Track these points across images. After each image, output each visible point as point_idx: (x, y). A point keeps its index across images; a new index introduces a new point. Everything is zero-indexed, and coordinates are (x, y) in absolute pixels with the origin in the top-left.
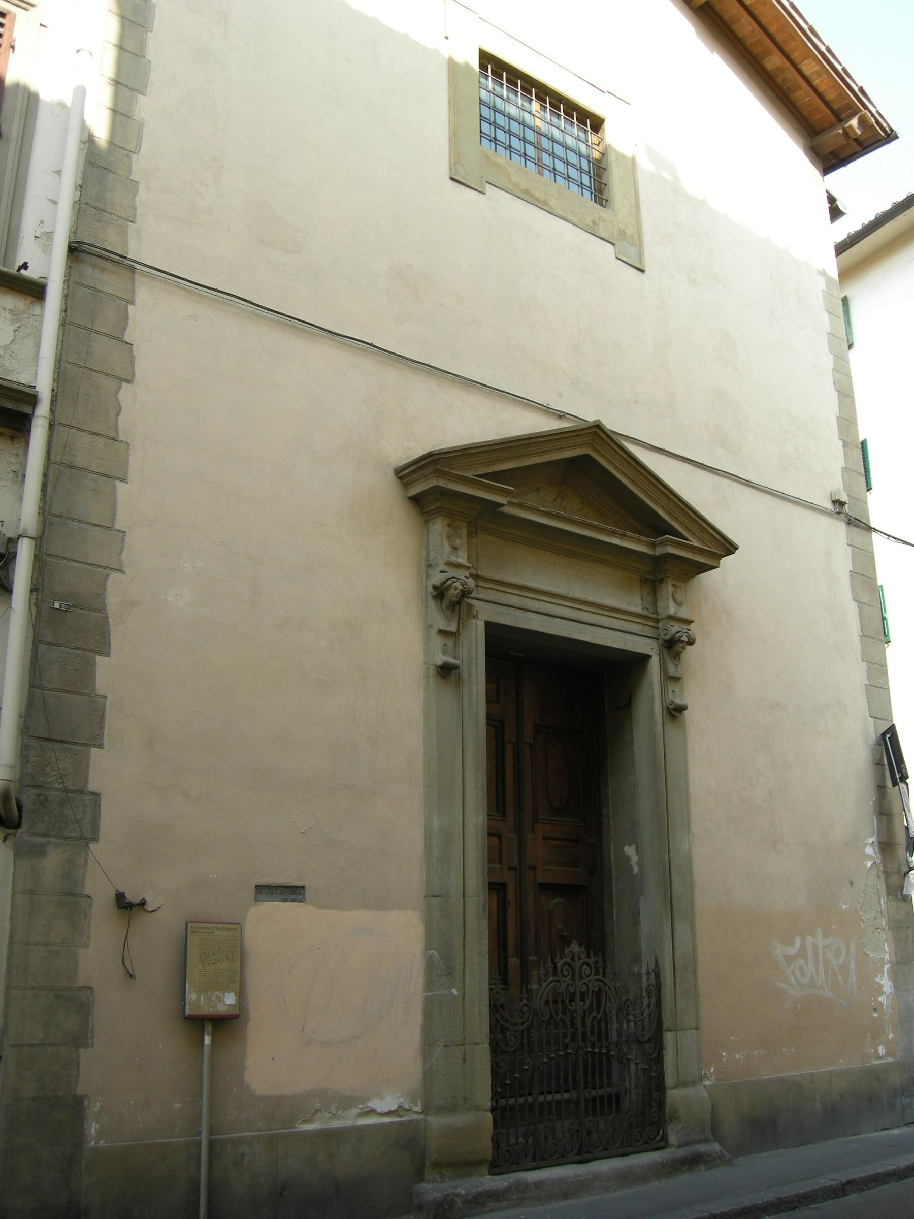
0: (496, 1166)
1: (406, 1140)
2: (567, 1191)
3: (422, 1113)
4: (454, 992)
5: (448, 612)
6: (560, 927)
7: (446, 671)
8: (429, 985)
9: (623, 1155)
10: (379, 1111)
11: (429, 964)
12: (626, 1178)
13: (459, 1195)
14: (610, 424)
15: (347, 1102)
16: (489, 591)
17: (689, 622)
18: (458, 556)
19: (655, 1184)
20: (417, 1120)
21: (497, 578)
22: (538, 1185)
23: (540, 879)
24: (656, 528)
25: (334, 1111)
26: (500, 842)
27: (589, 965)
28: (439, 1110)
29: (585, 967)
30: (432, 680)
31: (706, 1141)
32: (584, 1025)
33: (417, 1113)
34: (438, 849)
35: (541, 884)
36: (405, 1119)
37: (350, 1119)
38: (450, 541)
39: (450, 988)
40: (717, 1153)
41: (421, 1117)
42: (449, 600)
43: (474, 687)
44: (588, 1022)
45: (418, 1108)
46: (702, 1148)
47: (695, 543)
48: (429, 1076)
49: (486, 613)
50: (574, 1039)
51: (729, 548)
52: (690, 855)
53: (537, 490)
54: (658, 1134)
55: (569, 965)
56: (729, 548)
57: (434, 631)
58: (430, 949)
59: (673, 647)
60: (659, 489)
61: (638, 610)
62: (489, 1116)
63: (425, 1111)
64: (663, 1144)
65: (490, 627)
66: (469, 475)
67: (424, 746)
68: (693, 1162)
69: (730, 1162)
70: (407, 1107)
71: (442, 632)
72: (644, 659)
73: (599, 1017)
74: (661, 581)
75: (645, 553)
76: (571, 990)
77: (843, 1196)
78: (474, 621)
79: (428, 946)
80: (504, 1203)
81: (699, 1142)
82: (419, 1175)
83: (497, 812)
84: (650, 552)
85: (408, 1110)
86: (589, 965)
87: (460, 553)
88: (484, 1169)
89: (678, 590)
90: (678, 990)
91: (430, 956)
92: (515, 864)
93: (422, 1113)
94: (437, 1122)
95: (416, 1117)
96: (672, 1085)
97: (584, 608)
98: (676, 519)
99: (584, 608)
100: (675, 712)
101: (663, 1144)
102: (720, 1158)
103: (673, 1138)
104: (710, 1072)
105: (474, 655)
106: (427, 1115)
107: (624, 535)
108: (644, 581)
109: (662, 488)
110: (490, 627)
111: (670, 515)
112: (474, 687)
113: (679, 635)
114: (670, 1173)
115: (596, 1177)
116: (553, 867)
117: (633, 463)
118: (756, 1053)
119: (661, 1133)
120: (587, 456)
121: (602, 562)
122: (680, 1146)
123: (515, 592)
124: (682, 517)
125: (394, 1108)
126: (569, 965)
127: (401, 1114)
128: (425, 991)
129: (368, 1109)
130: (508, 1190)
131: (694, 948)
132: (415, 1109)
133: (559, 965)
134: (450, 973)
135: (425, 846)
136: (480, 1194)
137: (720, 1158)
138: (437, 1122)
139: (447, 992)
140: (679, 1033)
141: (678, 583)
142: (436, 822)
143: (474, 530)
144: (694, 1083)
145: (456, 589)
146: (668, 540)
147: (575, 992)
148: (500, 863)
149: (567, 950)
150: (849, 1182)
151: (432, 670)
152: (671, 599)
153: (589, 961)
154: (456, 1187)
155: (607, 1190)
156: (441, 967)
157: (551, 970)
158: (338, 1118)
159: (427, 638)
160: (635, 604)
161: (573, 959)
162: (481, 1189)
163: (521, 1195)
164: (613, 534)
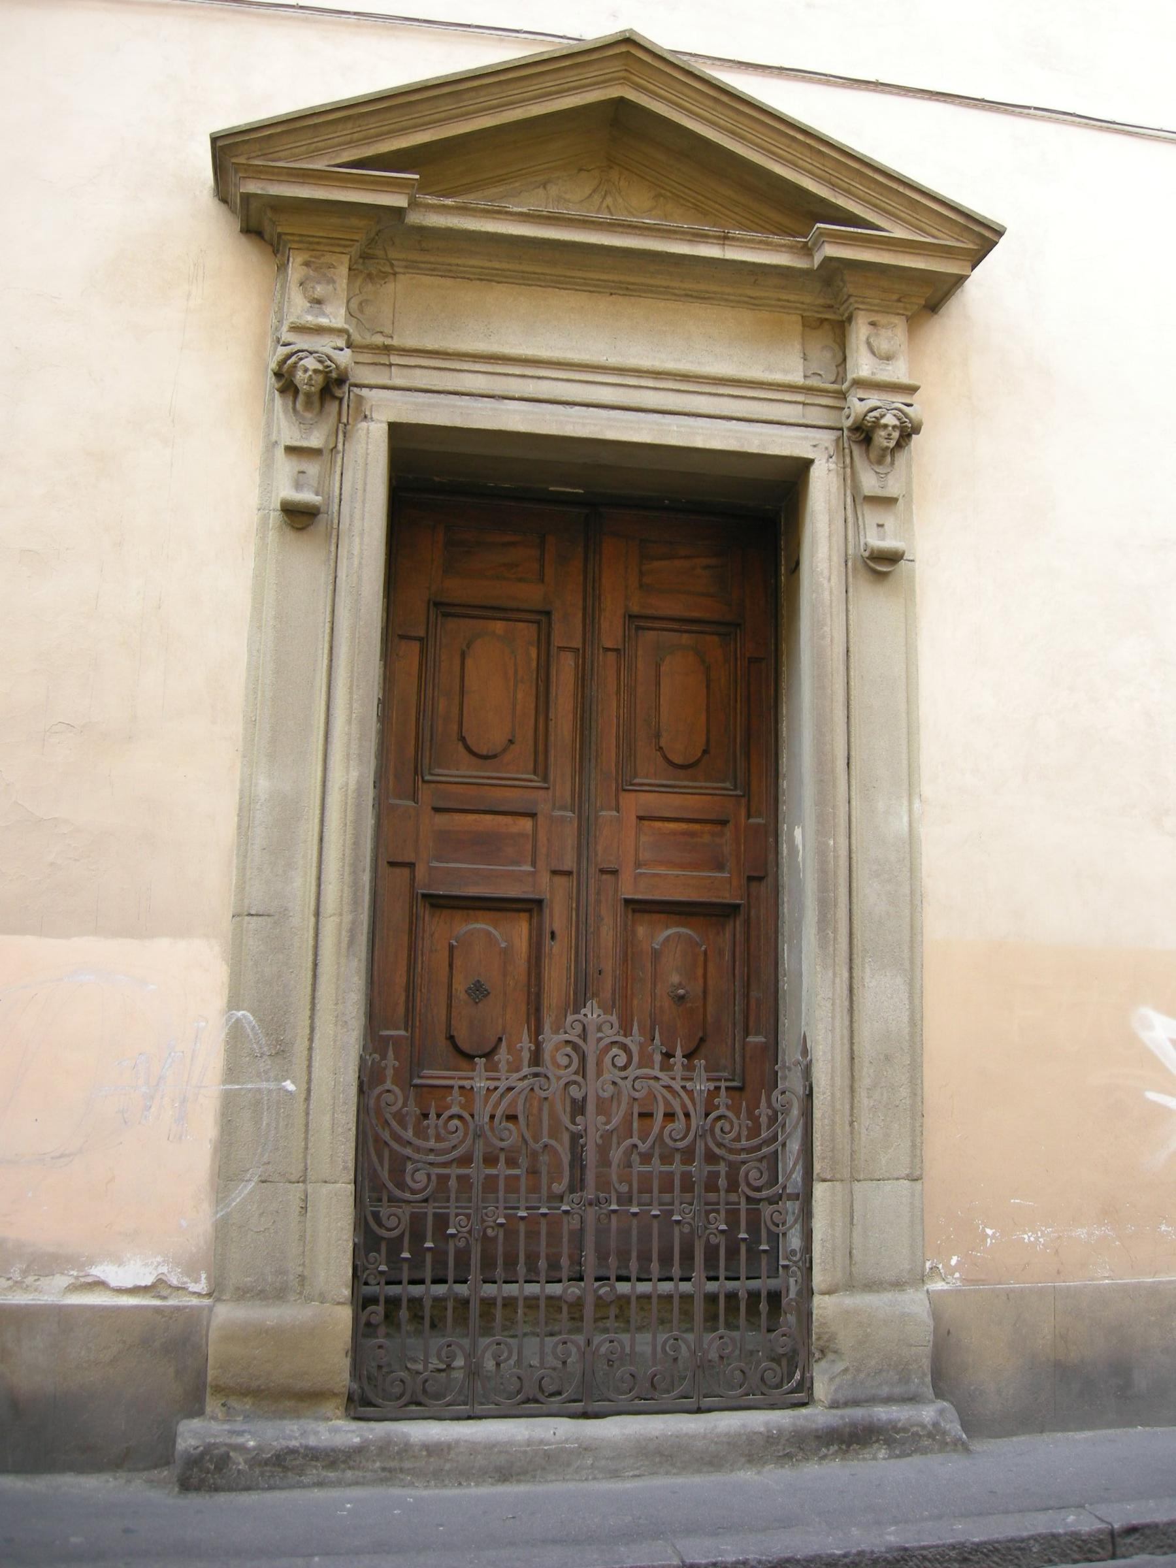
0: (360, 1404)
1: (169, 1343)
2: (507, 1467)
3: (209, 1295)
4: (289, 1085)
5: (308, 415)
6: (675, 979)
7: (299, 517)
8: (232, 1072)
9: (699, 1411)
10: (113, 1283)
11: (236, 1034)
12: (713, 1457)
13: (241, 1448)
14: (665, 35)
15: (45, 1263)
16: (418, 372)
17: (912, 390)
18: (324, 315)
19: (747, 1475)
20: (192, 1308)
21: (430, 345)
22: (433, 1450)
23: (628, 891)
24: (800, 212)
25: (17, 1277)
26: (535, 827)
27: (624, 1047)
28: (243, 1294)
29: (615, 1051)
30: (272, 536)
31: (912, 1399)
32: (604, 1161)
33: (199, 1295)
34: (266, 834)
35: (628, 902)
36: (171, 1302)
37: (52, 1291)
38: (305, 291)
39: (278, 1079)
40: (923, 1426)
41: (207, 1302)
42: (315, 393)
43: (357, 540)
44: (616, 1155)
45: (202, 1286)
46: (883, 1413)
47: (899, 233)
48: (223, 1231)
49: (385, 408)
50: (576, 1185)
51: (981, 237)
52: (912, 841)
53: (544, 185)
54: (791, 1376)
55: (575, 1047)
56: (981, 237)
57: (280, 452)
58: (238, 1010)
59: (875, 440)
60: (794, 139)
61: (797, 378)
62: (345, 1314)
63: (215, 1292)
64: (802, 1396)
65: (395, 430)
66: (319, 165)
67: (250, 651)
68: (852, 1439)
69: (960, 1446)
70: (175, 1282)
71: (291, 450)
72: (795, 473)
73: (643, 1147)
74: (850, 319)
75: (788, 268)
76: (574, 1091)
77: (1114, 1556)
78: (364, 425)
79: (234, 1003)
80: (349, 1474)
81: (888, 1400)
82: (194, 1405)
83: (535, 773)
84: (800, 263)
85: (178, 1288)
86: (624, 1047)
87: (328, 309)
88: (332, 1407)
89: (883, 332)
90: (864, 1101)
91: (238, 1020)
92: (569, 863)
93: (209, 1295)
94: (226, 1313)
95: (195, 1301)
96: (823, 1287)
97: (651, 383)
98: (848, 193)
99: (651, 383)
100: (882, 565)
101: (802, 1396)
102: (930, 1435)
103: (821, 1389)
104: (947, 1264)
105: (360, 486)
106: (218, 1300)
107: (726, 238)
108: (811, 325)
109: (800, 137)
110: (395, 430)
111: (834, 186)
112: (357, 540)
113: (875, 414)
114: (789, 1456)
115: (587, 1448)
116: (661, 870)
117: (725, 99)
118: (1081, 1233)
119: (798, 1376)
120: (622, 100)
121: (702, 298)
122: (835, 1405)
123: (477, 367)
124: (858, 186)
125: (148, 1281)
126: (575, 1047)
127: (164, 1293)
128: (225, 1082)
129: (90, 1280)
130: (360, 1450)
131: (915, 1022)
132: (193, 1287)
133: (548, 1047)
134: (281, 1051)
135: (239, 827)
136: (293, 1451)
137: (930, 1435)
138: (226, 1313)
139: (272, 1086)
140: (857, 1186)
141: (881, 319)
142: (263, 784)
143: (388, 269)
144: (898, 1285)
145: (306, 370)
146: (822, 233)
147: (584, 1099)
148: (534, 864)
149: (570, 1018)
150: (1132, 1530)
151: (275, 516)
152: (863, 349)
153: (627, 1041)
154: (240, 1433)
155: (615, 1474)
156: (262, 1038)
157: (526, 1055)
158: (26, 1289)
159: (268, 464)
160: (789, 366)
161: (584, 1035)
162: (294, 1443)
163: (395, 1464)
164: (699, 237)
